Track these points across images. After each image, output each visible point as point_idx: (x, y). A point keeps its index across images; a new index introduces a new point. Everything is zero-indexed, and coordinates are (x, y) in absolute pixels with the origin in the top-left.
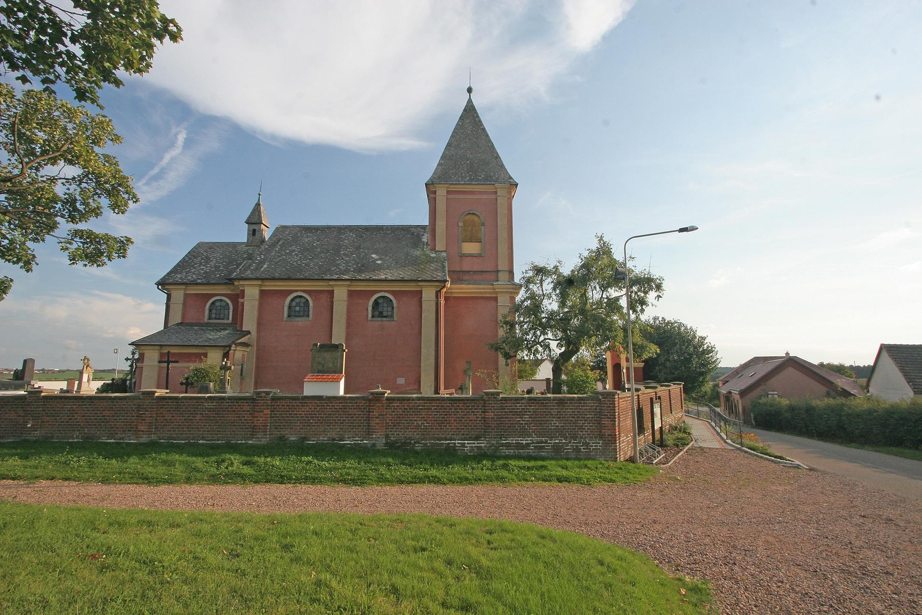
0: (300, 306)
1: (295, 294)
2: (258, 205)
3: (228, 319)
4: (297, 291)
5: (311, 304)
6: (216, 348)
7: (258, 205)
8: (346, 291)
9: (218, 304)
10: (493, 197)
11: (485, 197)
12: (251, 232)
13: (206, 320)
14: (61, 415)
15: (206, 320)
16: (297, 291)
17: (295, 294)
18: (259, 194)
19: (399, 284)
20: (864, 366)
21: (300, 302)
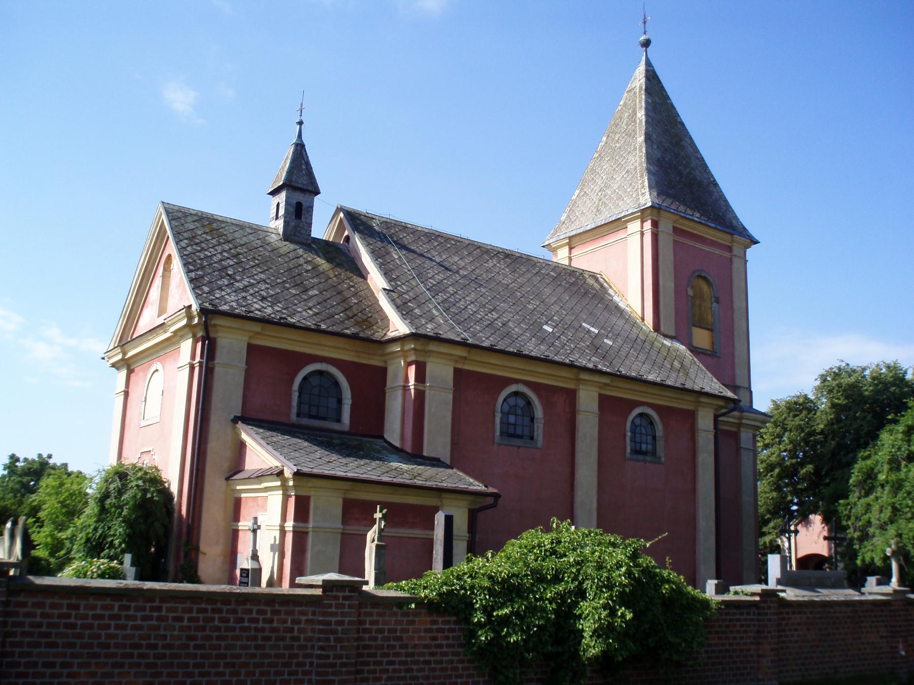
0: (516, 415)
1: (513, 388)
2: (300, 149)
3: (339, 420)
4: (517, 381)
5: (539, 412)
6: (459, 496)
7: (300, 149)
8: (596, 395)
9: (315, 381)
10: (727, 254)
11: (718, 252)
12: (292, 210)
13: (294, 418)
14: (100, 671)
15: (294, 418)
16: (517, 381)
17: (513, 388)
18: (301, 123)
19: (673, 395)
20: (65, 465)
21: (516, 406)
